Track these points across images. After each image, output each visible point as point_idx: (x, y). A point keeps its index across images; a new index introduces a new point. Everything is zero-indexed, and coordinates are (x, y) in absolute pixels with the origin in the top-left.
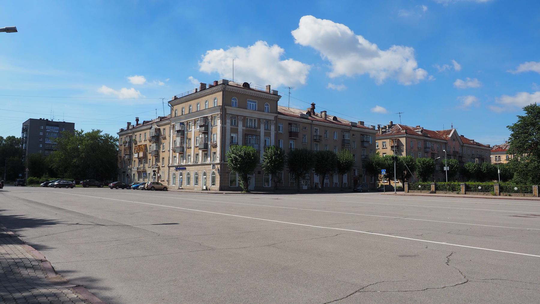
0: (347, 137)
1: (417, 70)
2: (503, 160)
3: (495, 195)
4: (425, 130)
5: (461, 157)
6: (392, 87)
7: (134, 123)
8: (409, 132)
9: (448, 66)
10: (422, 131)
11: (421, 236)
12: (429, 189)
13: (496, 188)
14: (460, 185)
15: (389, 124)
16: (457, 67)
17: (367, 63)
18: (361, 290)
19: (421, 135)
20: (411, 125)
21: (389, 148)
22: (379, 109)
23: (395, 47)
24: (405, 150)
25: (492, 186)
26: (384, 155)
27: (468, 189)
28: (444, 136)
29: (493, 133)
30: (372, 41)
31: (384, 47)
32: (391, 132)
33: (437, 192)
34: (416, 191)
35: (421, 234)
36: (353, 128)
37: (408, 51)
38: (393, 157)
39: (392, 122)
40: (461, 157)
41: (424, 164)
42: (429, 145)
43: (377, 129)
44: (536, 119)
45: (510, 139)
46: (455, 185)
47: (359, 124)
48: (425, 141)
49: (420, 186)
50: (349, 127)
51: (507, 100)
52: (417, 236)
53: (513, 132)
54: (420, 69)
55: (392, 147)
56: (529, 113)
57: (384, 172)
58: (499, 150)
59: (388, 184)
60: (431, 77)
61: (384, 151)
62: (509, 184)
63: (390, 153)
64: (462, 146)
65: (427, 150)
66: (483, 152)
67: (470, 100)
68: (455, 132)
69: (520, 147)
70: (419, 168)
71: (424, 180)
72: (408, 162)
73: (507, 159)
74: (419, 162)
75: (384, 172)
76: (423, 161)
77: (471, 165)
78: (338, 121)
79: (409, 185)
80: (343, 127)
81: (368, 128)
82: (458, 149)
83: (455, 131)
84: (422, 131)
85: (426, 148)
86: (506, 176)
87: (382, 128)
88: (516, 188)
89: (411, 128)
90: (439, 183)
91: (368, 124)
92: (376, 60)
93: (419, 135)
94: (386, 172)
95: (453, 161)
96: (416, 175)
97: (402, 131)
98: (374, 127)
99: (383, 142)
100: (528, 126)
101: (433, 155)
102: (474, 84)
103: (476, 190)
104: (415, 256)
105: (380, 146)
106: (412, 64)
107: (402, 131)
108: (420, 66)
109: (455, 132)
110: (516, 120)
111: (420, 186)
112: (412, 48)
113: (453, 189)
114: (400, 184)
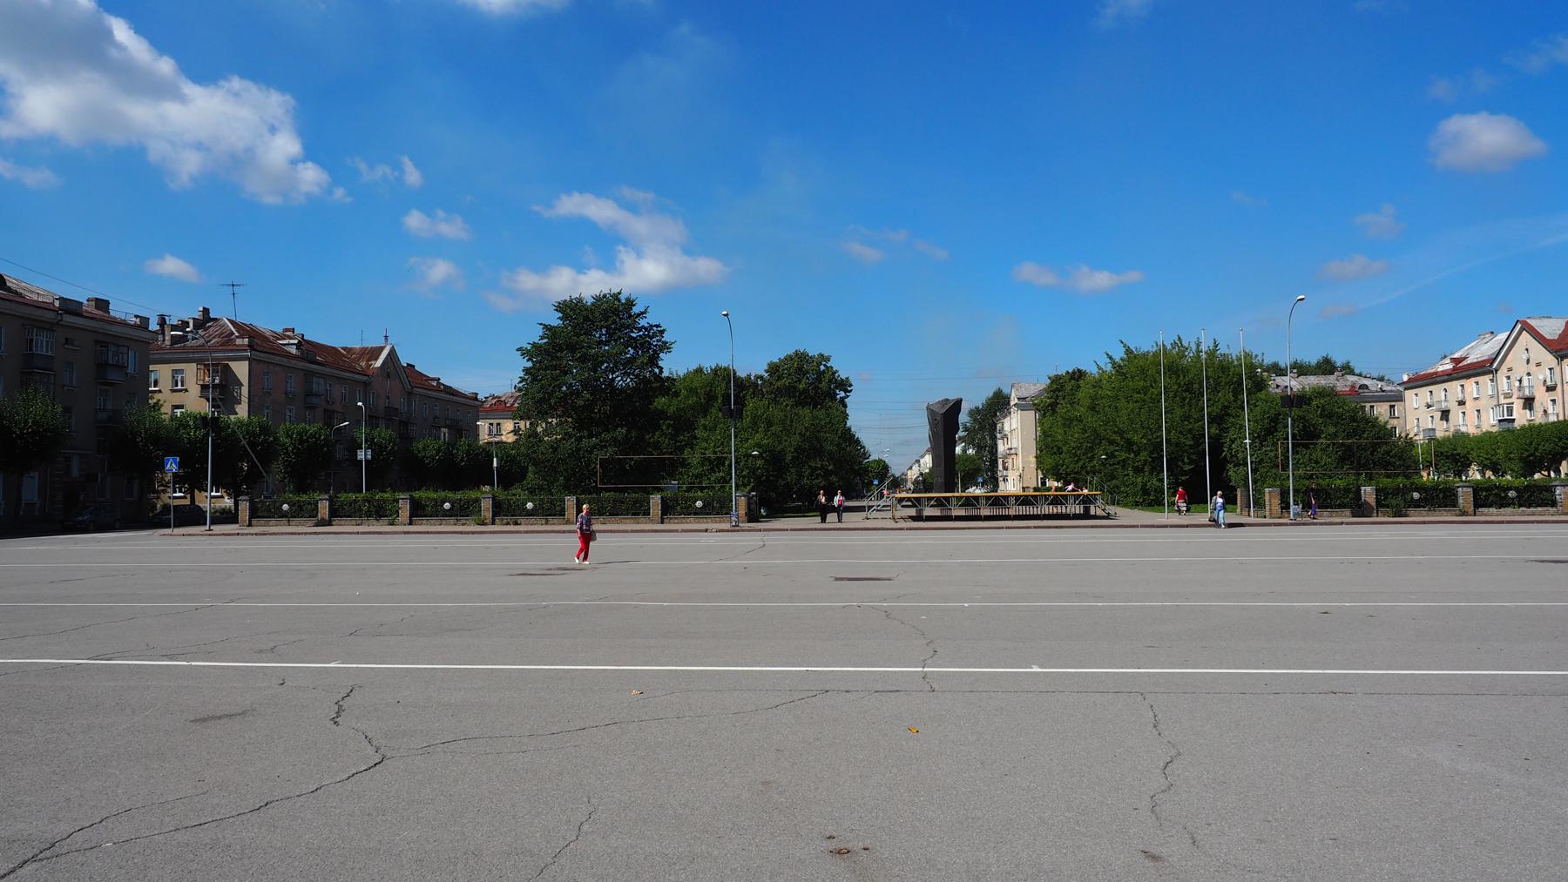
0: (43, 345)
1: (301, 166)
2: (508, 431)
3: (484, 524)
4: (308, 342)
5: (405, 424)
6: (216, 201)
7: (636, 310)
8: (259, 345)
9: (388, 171)
10: (299, 346)
11: (272, 652)
12: (313, 513)
13: (486, 505)
14: (397, 501)
15: (198, 315)
16: (413, 176)
17: (140, 113)
18: (48, 851)
19: (294, 357)
20: (268, 324)
21: (194, 390)
22: (171, 265)
23: (236, 83)
24: (245, 400)
25: (477, 501)
26: (178, 412)
27: (419, 511)
28: (363, 364)
29: (483, 365)
30: (160, 45)
31: (204, 72)
32: (201, 341)
33: (336, 520)
34: (273, 521)
35: (271, 645)
36: (68, 319)
37: (276, 103)
38: (204, 418)
39: (206, 311)
40: (405, 424)
41: (301, 441)
42: (318, 385)
43: (154, 326)
44: (578, 335)
45: (523, 380)
46: (385, 501)
47: (90, 308)
48: (309, 374)
49: (285, 507)
50: (51, 315)
51: (528, 281)
52: (260, 654)
53: (530, 364)
54: (310, 164)
55: (204, 387)
56: (565, 317)
57: (172, 466)
58: (498, 408)
59: (187, 502)
60: (339, 192)
61: (177, 399)
62: (518, 493)
63: (196, 403)
64: (410, 393)
65: (314, 400)
66: (461, 410)
67: (440, 270)
68: (392, 355)
69: (541, 401)
70: (287, 453)
71: (301, 488)
72: (254, 435)
73: (516, 431)
74: (288, 436)
75: (172, 466)
76: (299, 434)
77: (429, 446)
78: (9, 290)
79: (252, 502)
80: (28, 310)
81: (124, 323)
82: (399, 402)
83: (393, 351)
84: (299, 346)
85: (309, 394)
86: (511, 474)
87: (174, 328)
88: (530, 505)
89: (268, 334)
90: (343, 496)
91: (124, 309)
92: (172, 109)
93: (289, 356)
94: (180, 465)
95: (384, 433)
96: (276, 472)
97: (239, 341)
98: (145, 321)
99: (175, 372)
100: (561, 350)
101: (329, 417)
102: (451, 229)
103: (436, 513)
104: (244, 713)
105: (165, 383)
106: (285, 146)
107: (239, 341)
108: (311, 153)
109: (392, 355)
110: (535, 335)
111: (285, 507)
112: (288, 97)
113: (381, 512)
114: (228, 502)
